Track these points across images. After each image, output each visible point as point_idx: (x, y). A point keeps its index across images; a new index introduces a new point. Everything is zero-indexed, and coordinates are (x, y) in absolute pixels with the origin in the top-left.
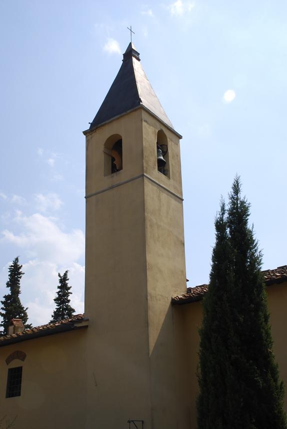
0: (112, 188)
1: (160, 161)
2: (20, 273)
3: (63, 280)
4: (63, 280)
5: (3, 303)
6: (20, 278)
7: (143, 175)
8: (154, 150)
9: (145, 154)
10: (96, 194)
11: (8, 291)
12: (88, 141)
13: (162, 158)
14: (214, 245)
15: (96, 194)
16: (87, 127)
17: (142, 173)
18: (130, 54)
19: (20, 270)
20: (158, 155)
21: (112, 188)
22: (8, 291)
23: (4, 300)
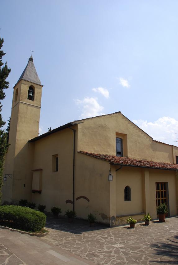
9: (21, 94)
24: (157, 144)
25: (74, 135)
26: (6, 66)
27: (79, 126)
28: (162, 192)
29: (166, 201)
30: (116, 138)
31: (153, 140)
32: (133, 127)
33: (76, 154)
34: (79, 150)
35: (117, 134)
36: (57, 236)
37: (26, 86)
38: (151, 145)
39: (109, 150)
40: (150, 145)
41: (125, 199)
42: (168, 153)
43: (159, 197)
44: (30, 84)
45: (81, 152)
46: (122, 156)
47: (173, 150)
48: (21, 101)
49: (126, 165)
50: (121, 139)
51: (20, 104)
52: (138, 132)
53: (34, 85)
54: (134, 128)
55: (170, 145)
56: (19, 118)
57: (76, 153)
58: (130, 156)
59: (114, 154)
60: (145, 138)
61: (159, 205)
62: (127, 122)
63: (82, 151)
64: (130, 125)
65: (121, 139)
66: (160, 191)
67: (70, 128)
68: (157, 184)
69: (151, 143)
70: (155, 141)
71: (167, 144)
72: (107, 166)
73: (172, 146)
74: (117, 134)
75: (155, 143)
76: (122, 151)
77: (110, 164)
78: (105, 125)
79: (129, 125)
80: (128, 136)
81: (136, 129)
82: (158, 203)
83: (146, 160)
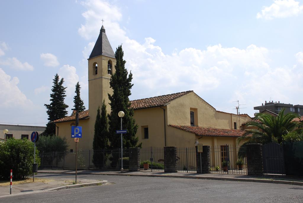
0: (95, 79)
1: (109, 71)
2: (80, 88)
3: (78, 87)
4: (78, 87)
5: (74, 98)
6: (80, 89)
7: (102, 77)
8: (106, 68)
9: (103, 70)
10: (91, 80)
11: (76, 94)
12: (89, 62)
13: (110, 69)
14: (285, 103)
15: (91, 80)
16: (88, 58)
17: (101, 77)
18: (102, 30)
19: (80, 87)
20: (108, 69)
21: (95, 79)
22: (76, 94)
23: (68, 113)
24: (219, 113)
25: (164, 113)
26: (131, 73)
27: (169, 107)
28: (224, 152)
29: (228, 160)
30: (190, 112)
31: (216, 111)
32: (201, 101)
33: (167, 127)
34: (168, 124)
35: (191, 109)
36: (76, 191)
37: (106, 61)
38: (215, 115)
39: (186, 122)
40: (214, 115)
41: (23, 135)
42: (228, 120)
43: (222, 156)
44: (109, 59)
45: (170, 125)
46: (194, 126)
47: (232, 117)
48: (103, 76)
49: (204, 136)
50: (193, 113)
51: (103, 79)
52: (205, 105)
53: (111, 59)
54: (202, 102)
55: (230, 114)
56: (103, 92)
57: (167, 127)
58: (200, 125)
59: (190, 125)
60: (210, 110)
61: (223, 161)
62: (198, 98)
63: (170, 124)
64: (200, 100)
65: (193, 113)
66: (223, 151)
67: (162, 108)
68: (222, 146)
69: (214, 113)
70: (218, 111)
71: (227, 113)
72: (193, 136)
73: (231, 114)
74: (191, 109)
75: (218, 113)
76: (194, 122)
77: (196, 135)
78: (184, 103)
79: (199, 100)
80: (198, 110)
81: (203, 103)
82: (222, 161)
83: (211, 127)
